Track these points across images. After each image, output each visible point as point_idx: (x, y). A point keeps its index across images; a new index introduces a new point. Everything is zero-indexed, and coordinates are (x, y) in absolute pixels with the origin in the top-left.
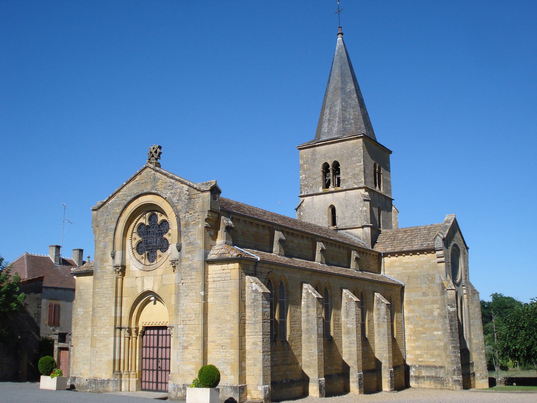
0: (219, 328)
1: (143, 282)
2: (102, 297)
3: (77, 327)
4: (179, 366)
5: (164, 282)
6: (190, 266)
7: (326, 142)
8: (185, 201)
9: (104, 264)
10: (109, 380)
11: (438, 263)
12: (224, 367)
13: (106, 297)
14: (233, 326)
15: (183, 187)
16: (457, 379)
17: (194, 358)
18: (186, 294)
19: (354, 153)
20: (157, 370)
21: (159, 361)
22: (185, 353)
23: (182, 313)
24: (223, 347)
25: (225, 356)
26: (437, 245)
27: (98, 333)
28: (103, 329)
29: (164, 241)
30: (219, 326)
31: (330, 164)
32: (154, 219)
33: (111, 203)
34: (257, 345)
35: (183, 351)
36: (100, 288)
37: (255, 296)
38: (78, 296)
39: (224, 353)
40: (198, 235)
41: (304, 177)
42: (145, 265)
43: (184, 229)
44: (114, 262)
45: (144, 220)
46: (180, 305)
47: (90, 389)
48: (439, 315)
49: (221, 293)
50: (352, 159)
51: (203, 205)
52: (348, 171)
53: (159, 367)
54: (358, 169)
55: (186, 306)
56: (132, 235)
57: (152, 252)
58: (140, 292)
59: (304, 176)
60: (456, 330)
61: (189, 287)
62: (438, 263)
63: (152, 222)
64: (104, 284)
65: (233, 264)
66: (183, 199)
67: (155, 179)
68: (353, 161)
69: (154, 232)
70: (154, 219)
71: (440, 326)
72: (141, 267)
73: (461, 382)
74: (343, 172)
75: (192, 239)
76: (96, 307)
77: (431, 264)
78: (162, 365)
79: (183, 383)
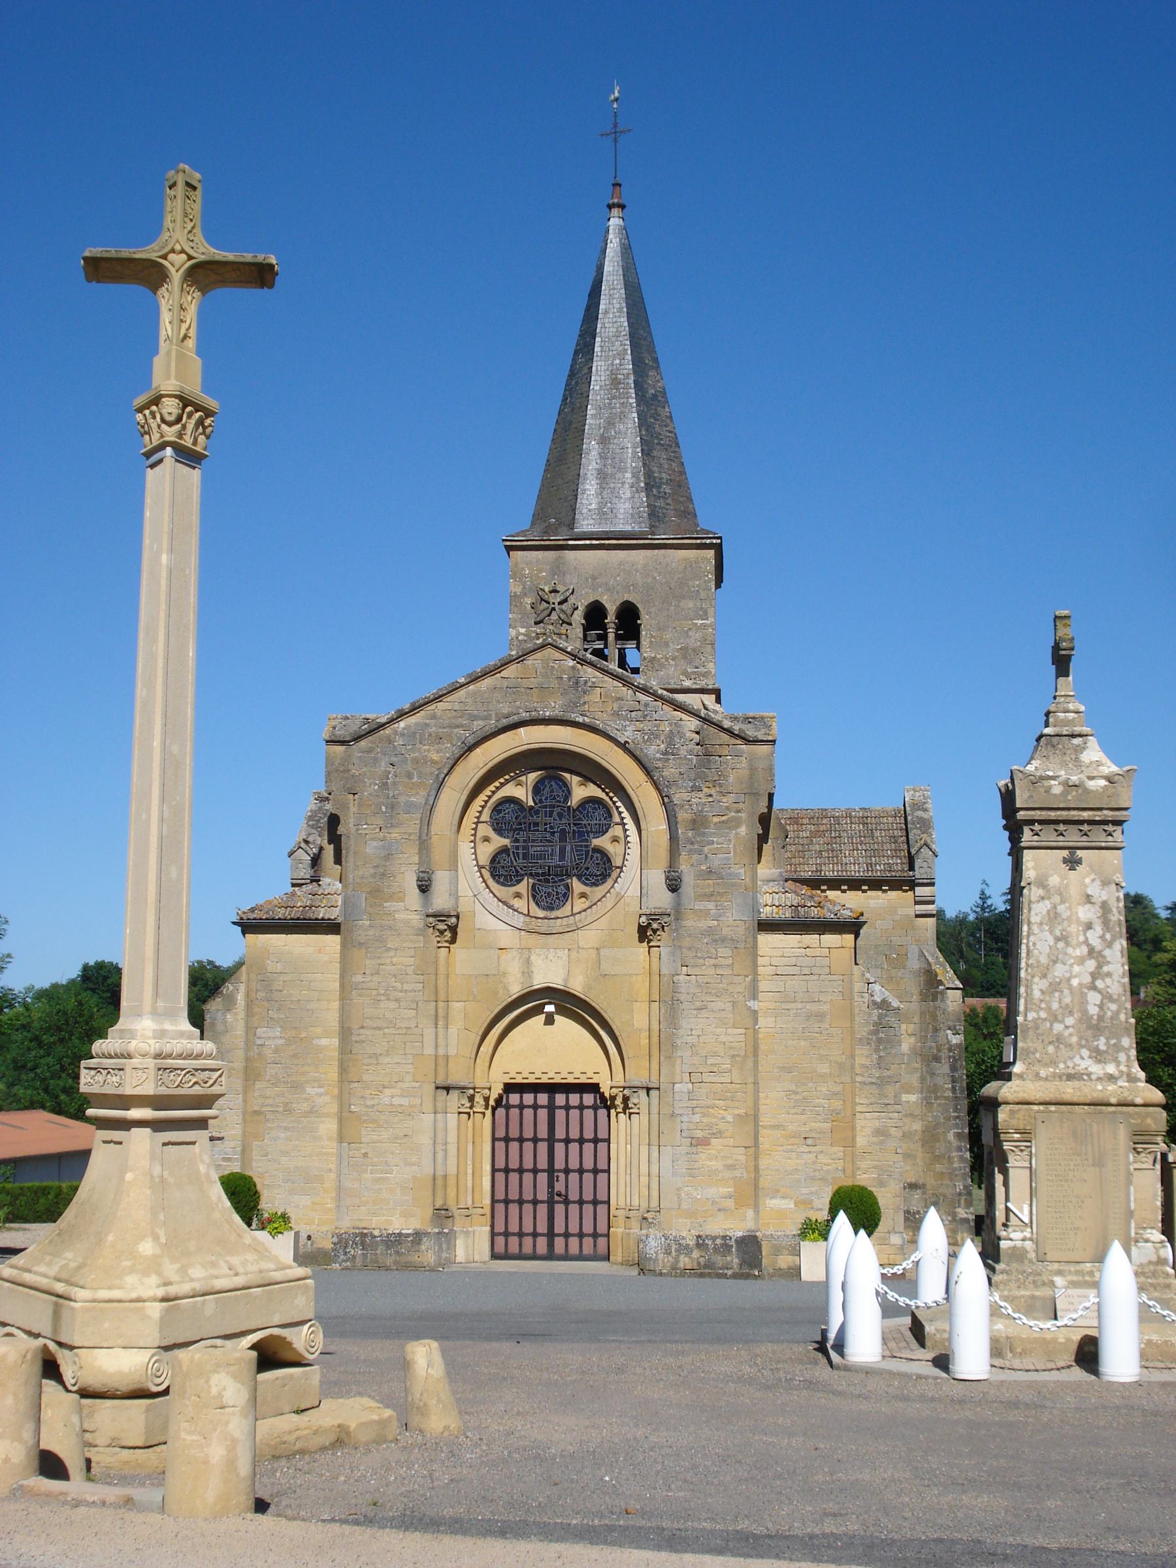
0: (796, 1093)
1: (528, 962)
2: (383, 998)
3: (257, 1082)
4: (679, 1189)
5: (606, 967)
6: (710, 931)
7: (603, 542)
8: (691, 760)
9: (385, 904)
10: (418, 1236)
11: (917, 916)
12: (813, 1189)
13: (397, 1000)
14: (839, 1088)
15: (681, 720)
16: (965, 1216)
17: (731, 1167)
18: (699, 1004)
19: (686, 589)
20: (551, 1203)
21: (558, 1177)
22: (701, 1155)
23: (689, 1053)
24: (809, 1141)
25: (814, 1163)
26: (922, 871)
27: (369, 1103)
28: (387, 1092)
29: (592, 856)
30: (794, 1088)
31: (611, 608)
32: (552, 791)
33: (404, 729)
34: (886, 1136)
35: (694, 1149)
36: (372, 974)
37: (880, 1016)
38: (257, 991)
39: (810, 1156)
40: (735, 853)
41: (522, 634)
42: (528, 915)
43: (690, 834)
44: (427, 902)
45: (521, 790)
46: (681, 1032)
47: (344, 1261)
48: (913, 1049)
49: (800, 1006)
50: (681, 604)
51: (751, 776)
52: (668, 636)
53: (559, 1195)
54: (698, 635)
55: (699, 1036)
56: (475, 829)
57: (547, 881)
58: (516, 990)
59: (523, 630)
60: (962, 1092)
61: (708, 988)
62: (917, 916)
63: (543, 798)
64: (388, 961)
65: (838, 937)
66: (683, 752)
67: (577, 683)
68: (682, 609)
69: (551, 828)
70: (552, 791)
71: (915, 1080)
72: (519, 921)
73: (972, 1224)
74: (652, 636)
75: (716, 861)
76: (355, 1026)
77: (897, 918)
78: (567, 1187)
79: (695, 1233)
